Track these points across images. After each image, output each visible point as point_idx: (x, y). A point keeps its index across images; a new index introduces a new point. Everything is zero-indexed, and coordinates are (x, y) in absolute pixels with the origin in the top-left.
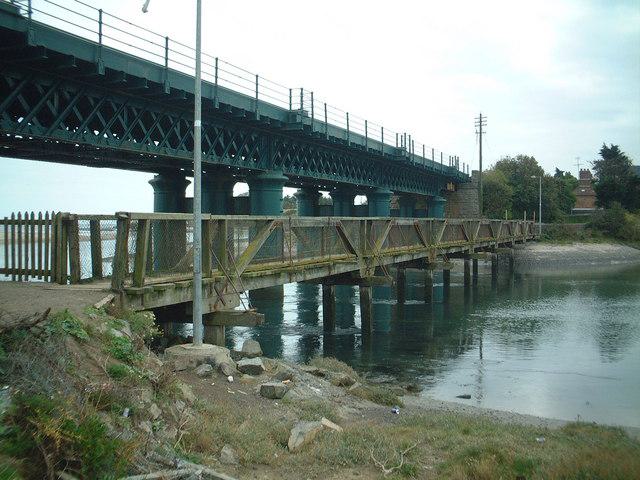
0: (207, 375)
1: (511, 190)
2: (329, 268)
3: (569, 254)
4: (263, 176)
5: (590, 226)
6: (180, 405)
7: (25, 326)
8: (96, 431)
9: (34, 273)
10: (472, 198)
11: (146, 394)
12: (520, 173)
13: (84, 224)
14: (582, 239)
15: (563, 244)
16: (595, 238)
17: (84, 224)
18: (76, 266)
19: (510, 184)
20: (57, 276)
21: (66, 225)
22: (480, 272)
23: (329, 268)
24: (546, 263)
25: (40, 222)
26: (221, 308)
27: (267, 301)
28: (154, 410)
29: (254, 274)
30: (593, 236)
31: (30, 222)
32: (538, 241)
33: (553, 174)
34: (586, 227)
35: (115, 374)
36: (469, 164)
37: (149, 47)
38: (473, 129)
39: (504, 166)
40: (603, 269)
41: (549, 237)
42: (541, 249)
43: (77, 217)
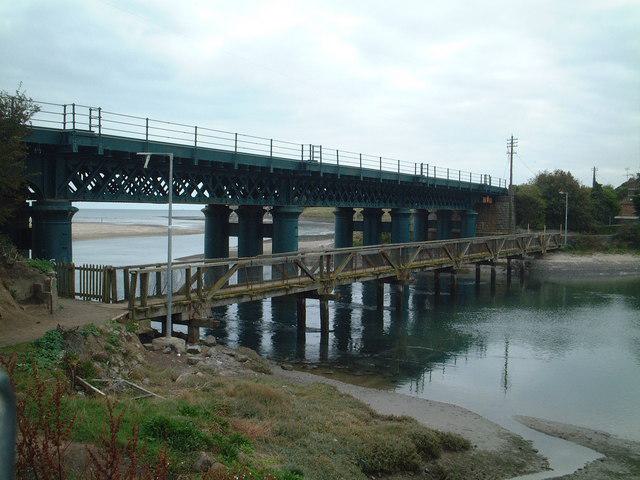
0: (168, 353)
1: (543, 203)
2: (287, 290)
3: (583, 266)
4: (282, 210)
5: (617, 237)
6: (135, 362)
7: (71, 332)
8: (90, 365)
9: (94, 296)
10: (507, 208)
11: (119, 358)
12: (556, 186)
13: (120, 275)
14: (605, 250)
15: (582, 255)
16: (620, 249)
17: (120, 275)
18: (115, 294)
19: (543, 197)
20: (106, 300)
21: (110, 272)
22: (498, 277)
23: (287, 290)
24: (557, 272)
25: (97, 270)
26: (196, 317)
27: (250, 312)
28: (122, 363)
29: (221, 297)
30: (619, 247)
31: (92, 269)
32: (562, 251)
33: (589, 184)
34: (613, 239)
35: (107, 349)
36: (499, 179)
37: (185, 136)
38: (506, 149)
39: (543, 179)
40: (614, 280)
41: (574, 247)
42: (561, 259)
43: (115, 268)
